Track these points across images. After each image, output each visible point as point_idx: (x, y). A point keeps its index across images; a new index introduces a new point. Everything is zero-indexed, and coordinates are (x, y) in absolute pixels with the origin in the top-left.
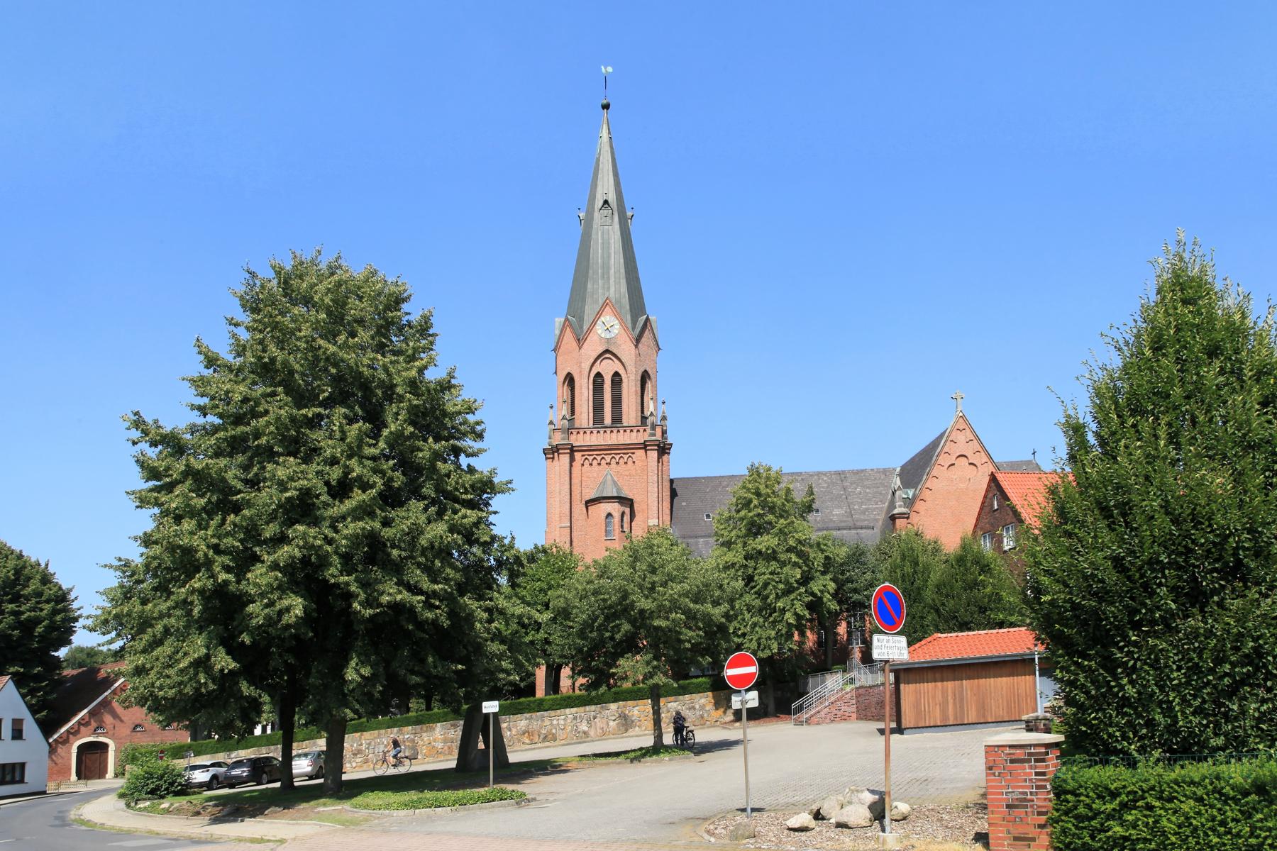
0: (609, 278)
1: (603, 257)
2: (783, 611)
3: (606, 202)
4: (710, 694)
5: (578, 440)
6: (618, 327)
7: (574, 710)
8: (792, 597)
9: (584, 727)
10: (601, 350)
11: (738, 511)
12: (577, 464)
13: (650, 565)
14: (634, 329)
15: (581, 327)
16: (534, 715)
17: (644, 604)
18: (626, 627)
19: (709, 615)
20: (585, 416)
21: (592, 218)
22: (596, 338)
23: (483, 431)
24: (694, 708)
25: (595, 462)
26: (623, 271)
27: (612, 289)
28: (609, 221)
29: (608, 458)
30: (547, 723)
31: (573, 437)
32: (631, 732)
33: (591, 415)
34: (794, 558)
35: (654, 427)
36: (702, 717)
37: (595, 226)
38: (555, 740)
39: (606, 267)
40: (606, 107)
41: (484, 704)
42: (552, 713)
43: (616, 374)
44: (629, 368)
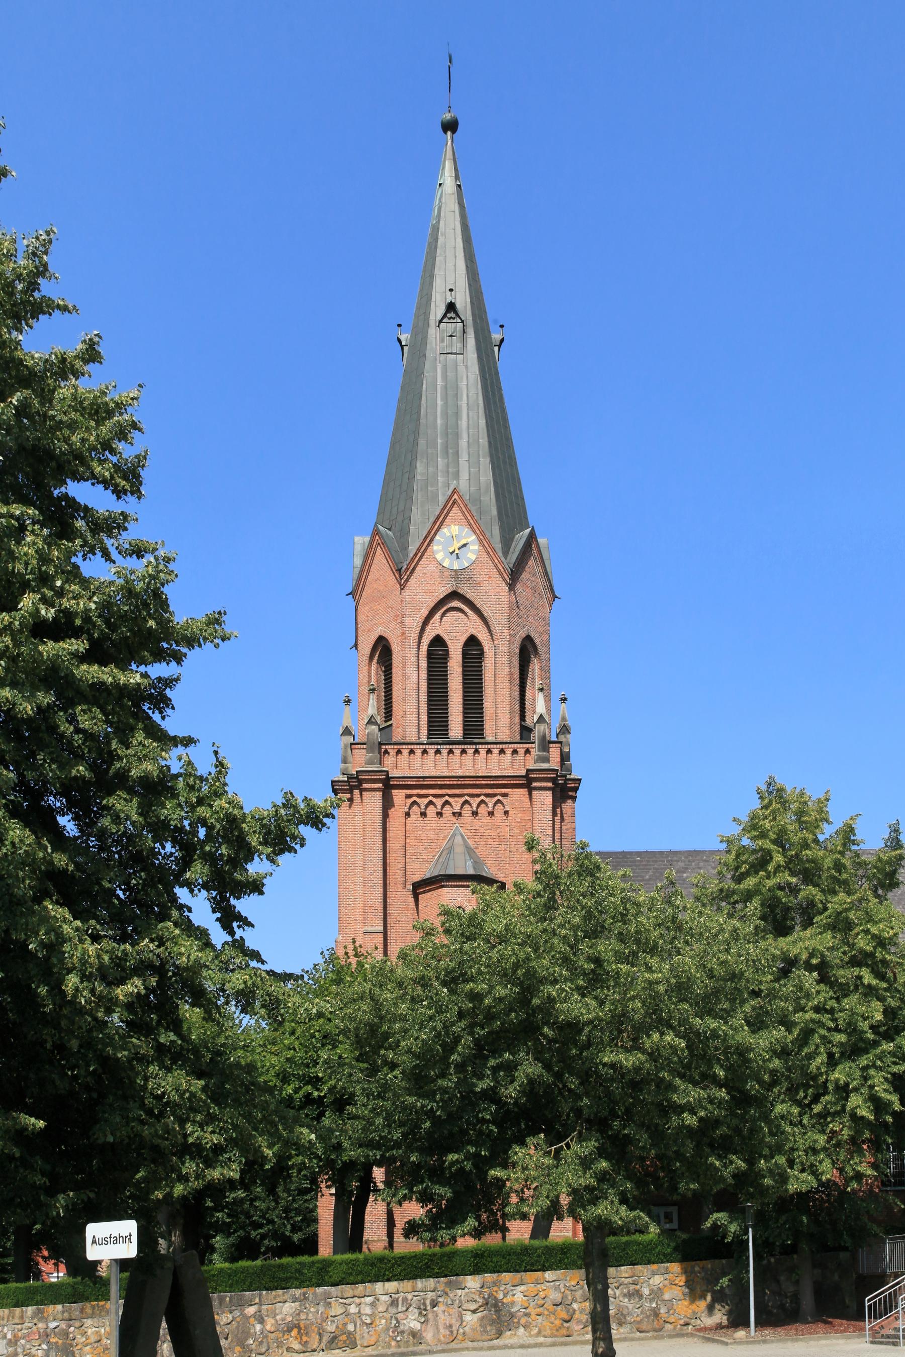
0: (457, 454)
1: (445, 414)
2: (844, 1091)
3: (451, 307)
4: (675, 1267)
5: (400, 766)
6: (475, 547)
7: (392, 1286)
8: (863, 1061)
9: (412, 1322)
10: (442, 591)
11: (739, 879)
12: (397, 813)
13: (589, 916)
14: (506, 553)
15: (405, 548)
16: (310, 1291)
17: (578, 1008)
18: (530, 1068)
19: (742, 1051)
20: (412, 719)
21: (425, 338)
22: (432, 567)
23: (141, 460)
24: (638, 1294)
25: (431, 811)
26: (484, 441)
27: (464, 476)
28: (457, 346)
29: (456, 804)
30: (336, 1309)
31: (389, 761)
32: (508, 1338)
33: (424, 718)
34: (868, 978)
35: (545, 744)
36: (656, 1313)
37: (430, 355)
38: (353, 1345)
39: (452, 434)
40: (450, 126)
41: (93, 1230)
42: (348, 1290)
43: (472, 642)
44: (496, 629)
